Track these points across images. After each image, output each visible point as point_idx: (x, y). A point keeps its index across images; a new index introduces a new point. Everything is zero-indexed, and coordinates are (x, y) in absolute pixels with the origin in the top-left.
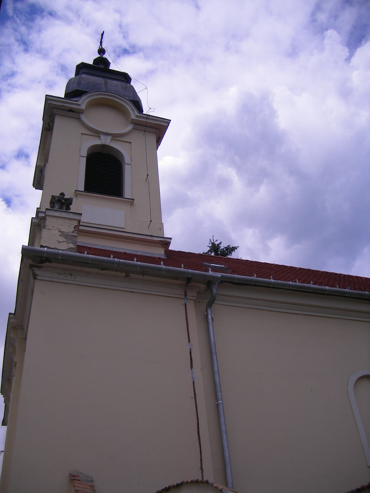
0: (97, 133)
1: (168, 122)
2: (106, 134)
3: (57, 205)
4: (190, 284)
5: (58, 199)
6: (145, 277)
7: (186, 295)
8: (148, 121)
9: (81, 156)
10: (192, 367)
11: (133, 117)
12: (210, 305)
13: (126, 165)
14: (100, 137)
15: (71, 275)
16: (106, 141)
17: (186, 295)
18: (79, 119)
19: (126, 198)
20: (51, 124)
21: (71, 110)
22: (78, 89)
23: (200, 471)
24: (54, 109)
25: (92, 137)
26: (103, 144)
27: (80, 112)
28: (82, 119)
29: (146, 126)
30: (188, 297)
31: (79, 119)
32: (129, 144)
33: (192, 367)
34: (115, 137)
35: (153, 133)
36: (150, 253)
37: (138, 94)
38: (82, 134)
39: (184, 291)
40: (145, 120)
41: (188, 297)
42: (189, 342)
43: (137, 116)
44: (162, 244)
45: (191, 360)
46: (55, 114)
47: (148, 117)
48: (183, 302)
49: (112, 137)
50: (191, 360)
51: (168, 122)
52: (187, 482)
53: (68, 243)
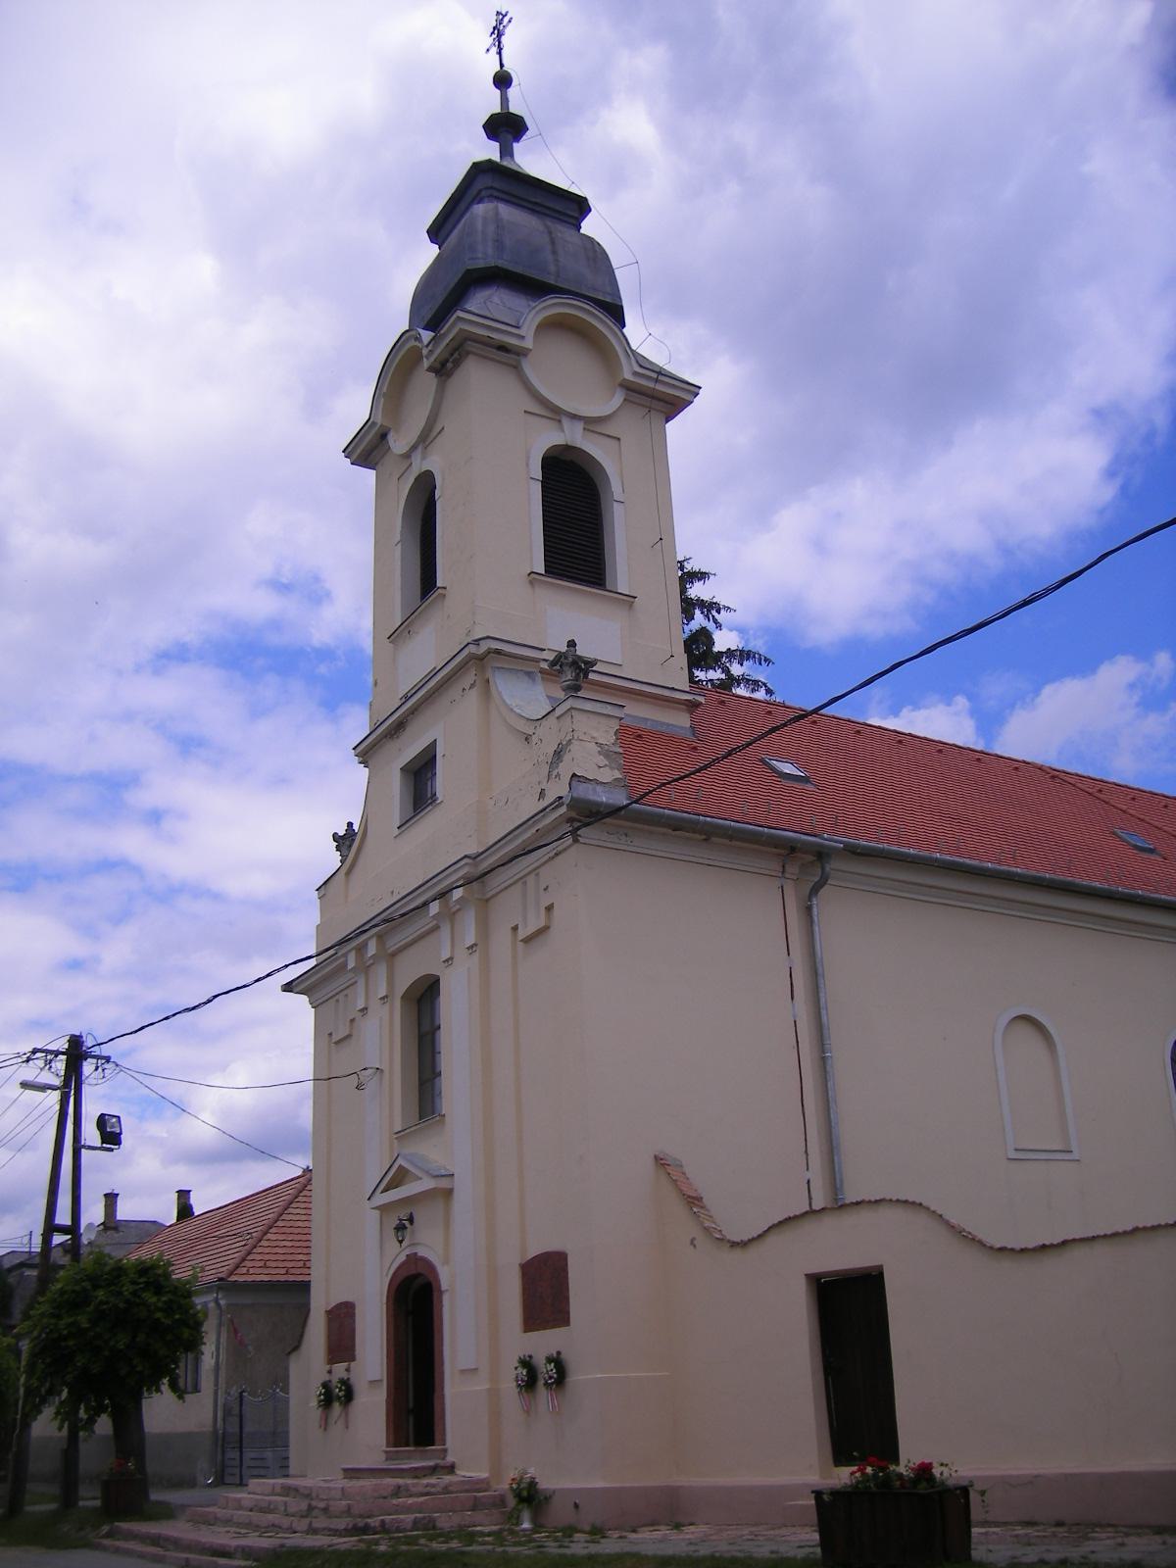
0: (556, 414)
1: (694, 390)
2: (574, 417)
3: (569, 672)
4: (795, 855)
5: (573, 660)
6: (734, 843)
7: (783, 872)
8: (659, 387)
9: (532, 478)
10: (792, 998)
11: (628, 376)
12: (815, 890)
13: (615, 504)
14: (560, 421)
15: (626, 835)
16: (573, 435)
17: (783, 872)
18: (516, 368)
19: (620, 594)
20: (449, 365)
21: (503, 348)
22: (500, 263)
23: (805, 1156)
24: (469, 343)
25: (544, 420)
26: (569, 444)
27: (522, 353)
28: (522, 369)
29: (653, 397)
30: (787, 876)
31: (516, 368)
32: (614, 443)
33: (792, 998)
34: (591, 423)
35: (662, 412)
36: (668, 725)
37: (617, 272)
38: (525, 412)
39: (781, 864)
40: (651, 385)
41: (787, 876)
42: (789, 954)
43: (635, 374)
44: (687, 706)
45: (792, 984)
46: (468, 353)
47: (661, 378)
48: (777, 883)
49: (585, 423)
50: (792, 984)
51: (694, 390)
52: (891, 1200)
53: (612, 768)
